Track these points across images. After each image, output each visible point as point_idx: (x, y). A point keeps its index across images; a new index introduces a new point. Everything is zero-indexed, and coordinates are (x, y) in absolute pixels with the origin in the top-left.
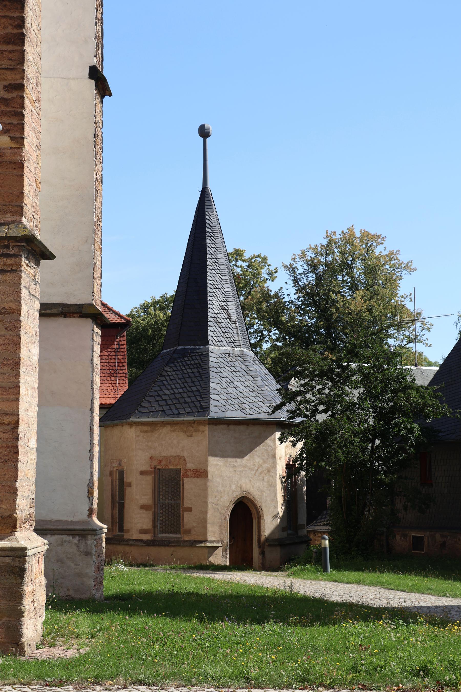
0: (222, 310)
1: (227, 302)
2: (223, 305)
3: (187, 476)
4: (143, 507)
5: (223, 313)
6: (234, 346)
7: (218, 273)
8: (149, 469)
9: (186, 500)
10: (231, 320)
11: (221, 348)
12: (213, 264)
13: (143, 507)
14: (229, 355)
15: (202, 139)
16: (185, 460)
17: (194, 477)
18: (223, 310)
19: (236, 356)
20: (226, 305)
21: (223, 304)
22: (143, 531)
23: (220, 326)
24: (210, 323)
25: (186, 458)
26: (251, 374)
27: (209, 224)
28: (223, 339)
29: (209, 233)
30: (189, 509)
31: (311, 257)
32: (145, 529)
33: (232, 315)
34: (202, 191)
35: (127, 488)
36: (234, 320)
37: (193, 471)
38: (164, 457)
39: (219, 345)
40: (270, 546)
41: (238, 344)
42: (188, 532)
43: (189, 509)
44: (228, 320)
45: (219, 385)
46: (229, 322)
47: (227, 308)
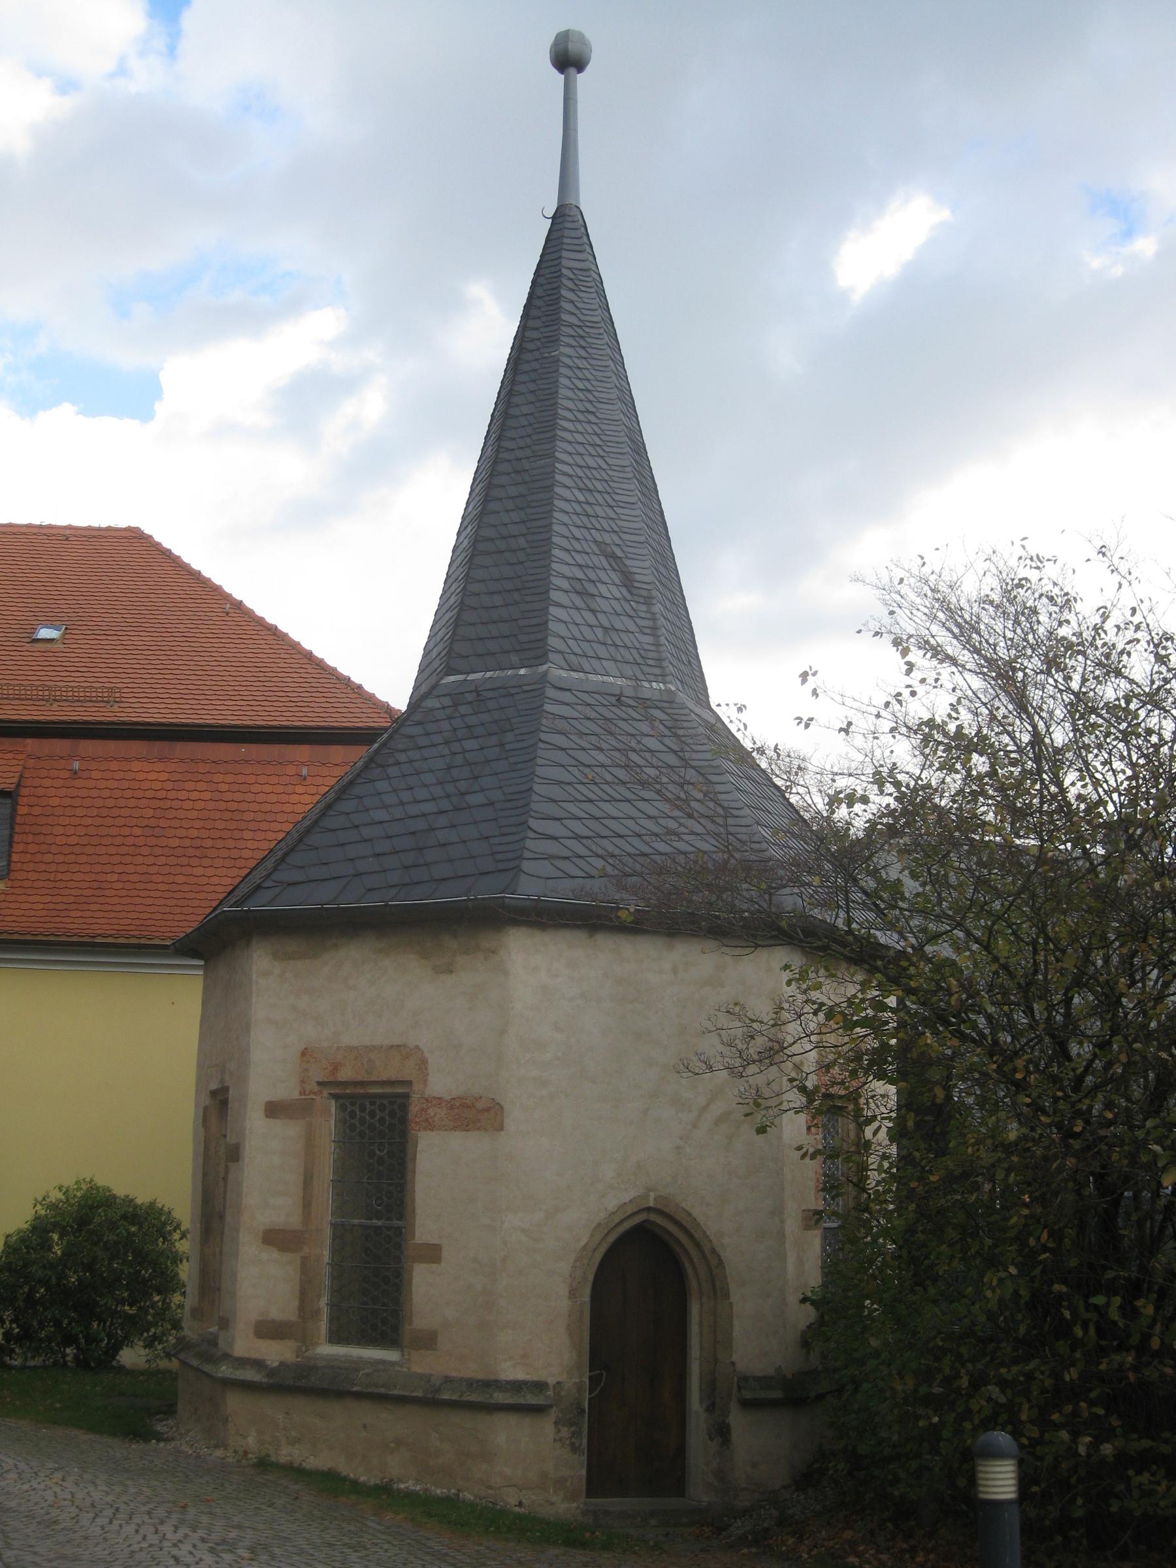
0: (603, 559)
1: (622, 535)
2: (608, 541)
3: (430, 1126)
4: (275, 1238)
5: (607, 566)
6: (641, 677)
7: (594, 445)
8: (295, 1095)
9: (419, 1221)
10: (635, 591)
11: (592, 677)
12: (580, 416)
13: (275, 1238)
14: (618, 700)
15: (561, 78)
16: (423, 1062)
17: (454, 1128)
18: (606, 557)
19: (645, 703)
20: (618, 541)
21: (607, 538)
22: (269, 1330)
23: (594, 606)
24: (555, 595)
25: (427, 1055)
26: (693, 763)
27: (572, 302)
28: (602, 651)
29: (571, 326)
30: (433, 1253)
31: (960, 728)
32: (273, 1321)
33: (638, 577)
34: (554, 218)
35: (419, 1134)
36: (645, 593)
37: (451, 1105)
38: (350, 1049)
39: (587, 667)
40: (746, 1404)
41: (657, 671)
42: (428, 1341)
43: (433, 1253)
44: (624, 590)
45: (568, 788)
46: (628, 596)
47: (619, 553)
